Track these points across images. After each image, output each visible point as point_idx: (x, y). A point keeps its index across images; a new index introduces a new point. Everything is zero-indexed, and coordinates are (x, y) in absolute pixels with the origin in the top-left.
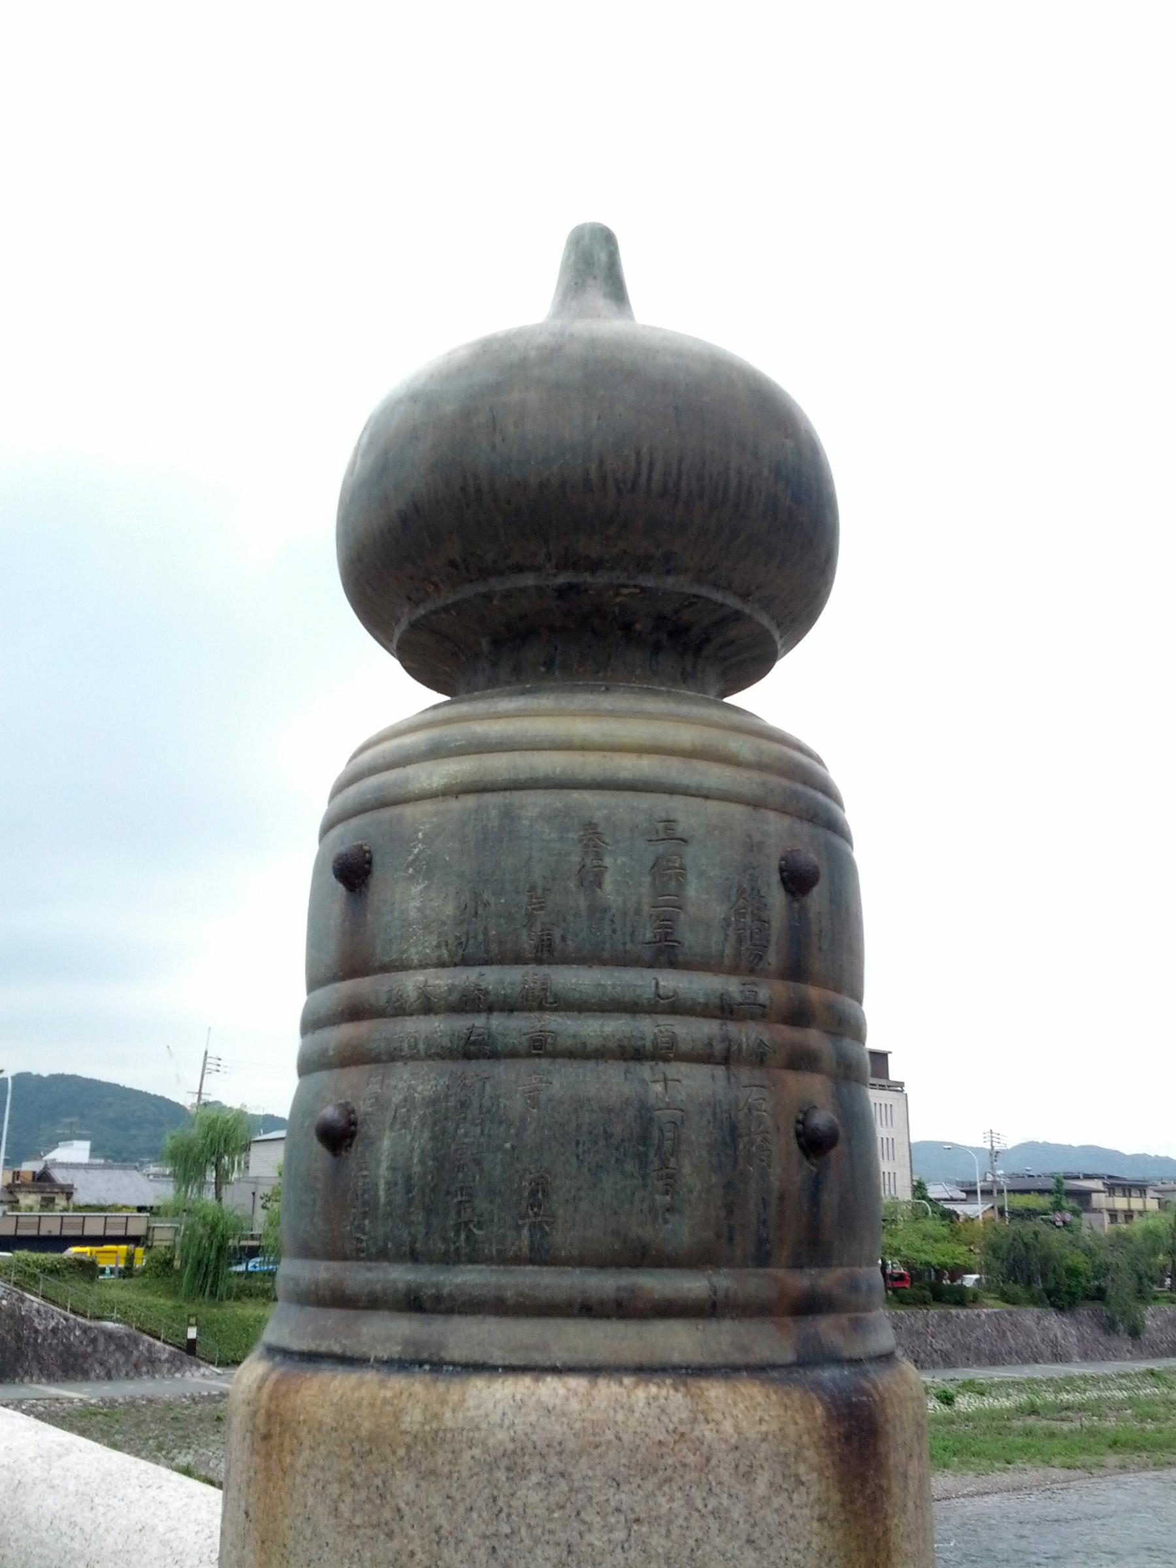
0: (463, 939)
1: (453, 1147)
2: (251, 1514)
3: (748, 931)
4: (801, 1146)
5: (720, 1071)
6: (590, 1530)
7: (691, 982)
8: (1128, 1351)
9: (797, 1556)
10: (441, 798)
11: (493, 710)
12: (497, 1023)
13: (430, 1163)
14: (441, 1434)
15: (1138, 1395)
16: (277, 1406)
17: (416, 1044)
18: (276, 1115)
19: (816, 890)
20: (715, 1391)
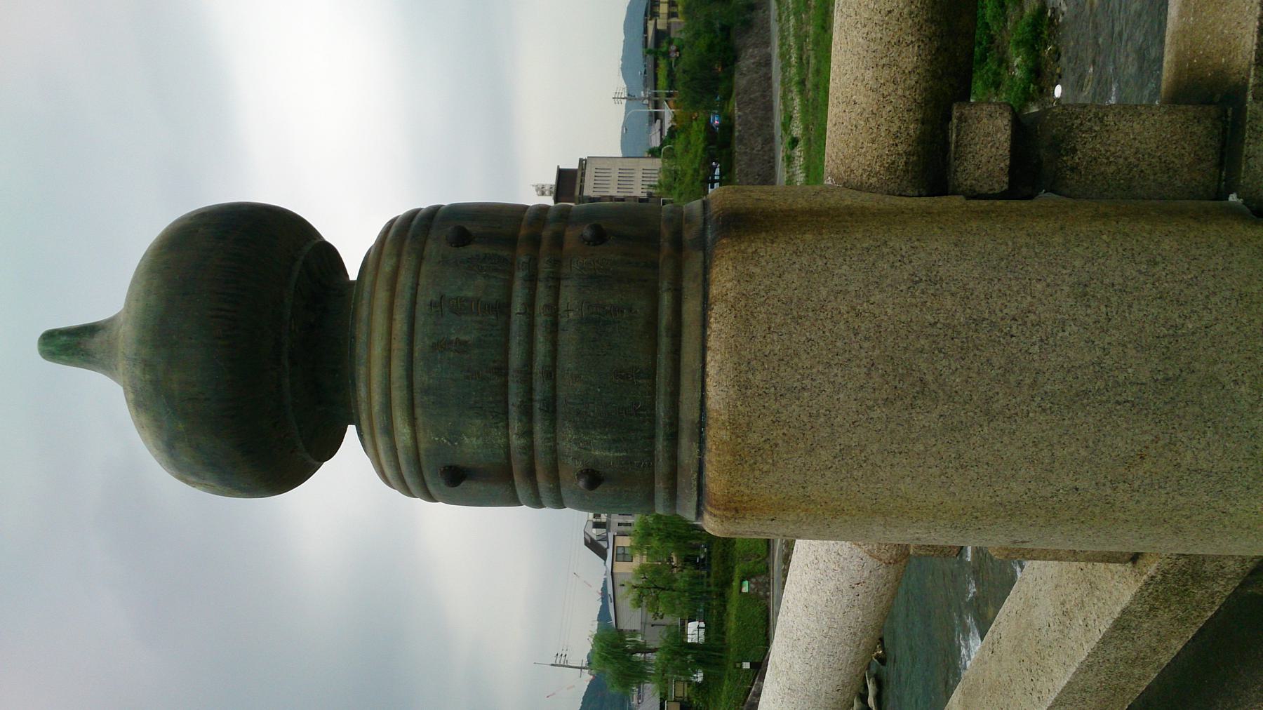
0: (494, 414)
1: (599, 418)
2: (772, 517)
3: (491, 265)
4: (601, 244)
5: (563, 283)
6: (773, 350)
7: (518, 296)
8: (764, 12)
9: (788, 255)
10: (416, 428)
11: (366, 400)
12: (538, 396)
13: (607, 429)
14: (731, 421)
15: (793, 8)
16: (722, 505)
17: (548, 438)
18: (598, 613)
19: (468, 228)
20: (714, 291)
